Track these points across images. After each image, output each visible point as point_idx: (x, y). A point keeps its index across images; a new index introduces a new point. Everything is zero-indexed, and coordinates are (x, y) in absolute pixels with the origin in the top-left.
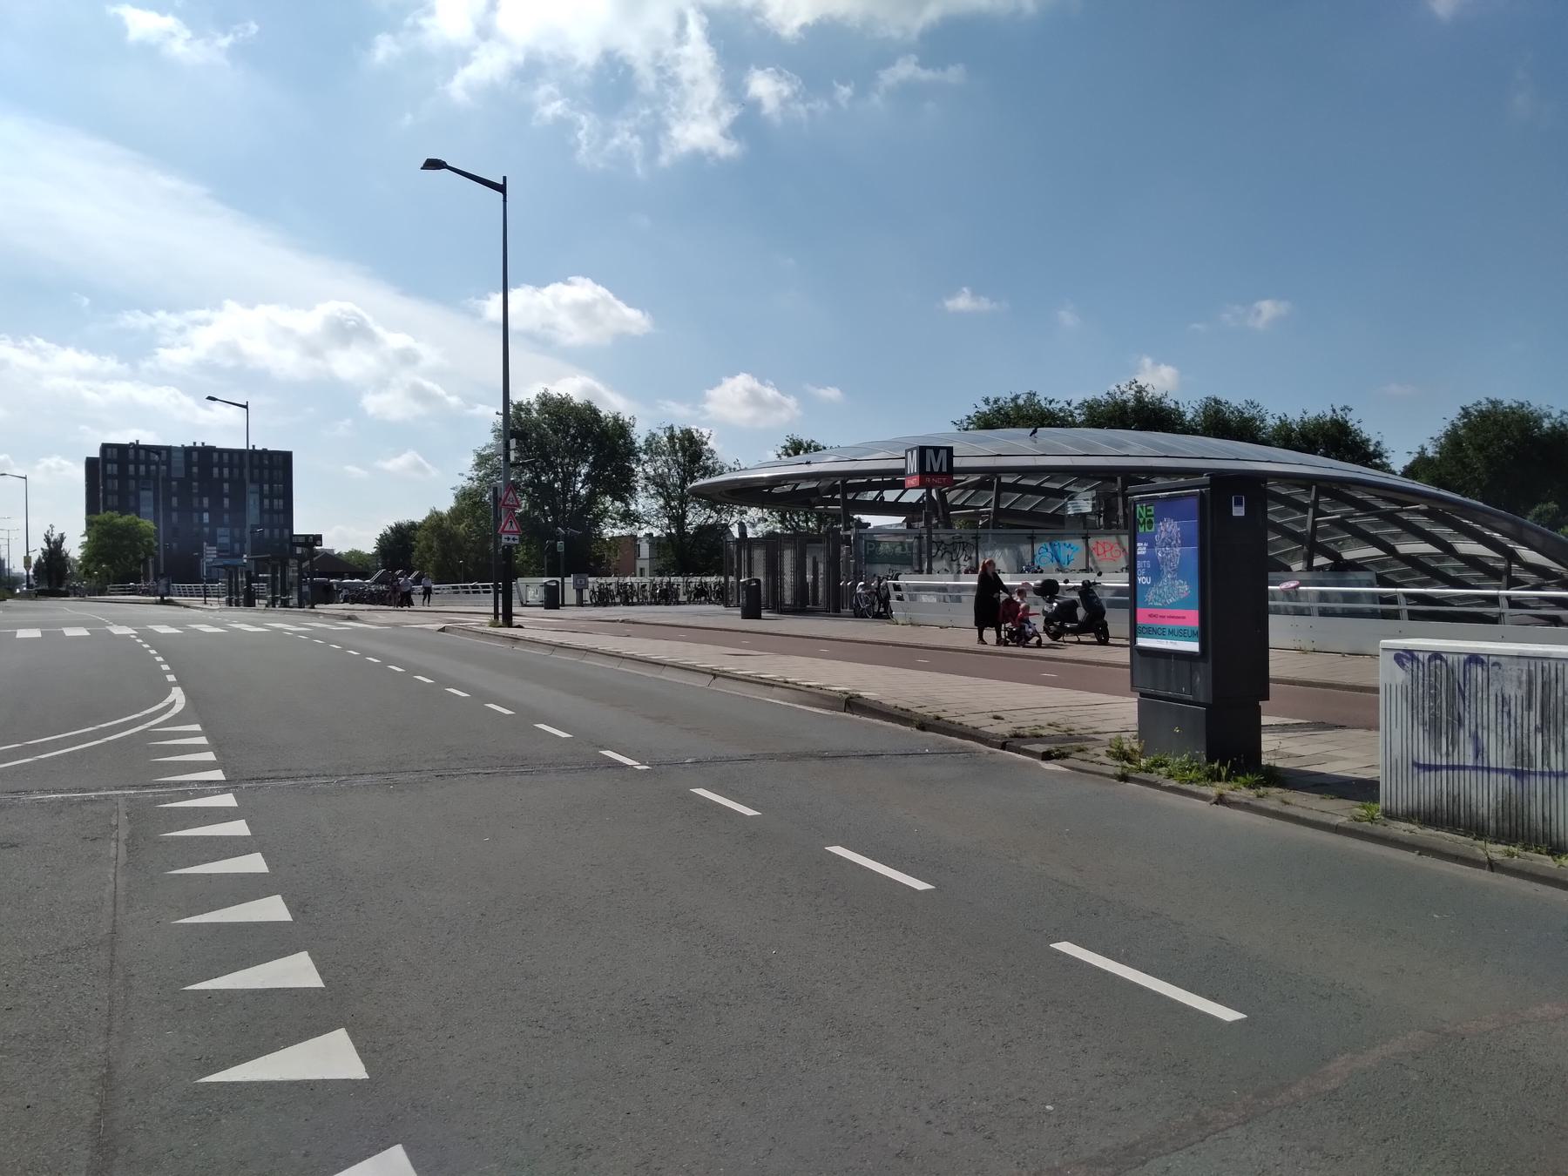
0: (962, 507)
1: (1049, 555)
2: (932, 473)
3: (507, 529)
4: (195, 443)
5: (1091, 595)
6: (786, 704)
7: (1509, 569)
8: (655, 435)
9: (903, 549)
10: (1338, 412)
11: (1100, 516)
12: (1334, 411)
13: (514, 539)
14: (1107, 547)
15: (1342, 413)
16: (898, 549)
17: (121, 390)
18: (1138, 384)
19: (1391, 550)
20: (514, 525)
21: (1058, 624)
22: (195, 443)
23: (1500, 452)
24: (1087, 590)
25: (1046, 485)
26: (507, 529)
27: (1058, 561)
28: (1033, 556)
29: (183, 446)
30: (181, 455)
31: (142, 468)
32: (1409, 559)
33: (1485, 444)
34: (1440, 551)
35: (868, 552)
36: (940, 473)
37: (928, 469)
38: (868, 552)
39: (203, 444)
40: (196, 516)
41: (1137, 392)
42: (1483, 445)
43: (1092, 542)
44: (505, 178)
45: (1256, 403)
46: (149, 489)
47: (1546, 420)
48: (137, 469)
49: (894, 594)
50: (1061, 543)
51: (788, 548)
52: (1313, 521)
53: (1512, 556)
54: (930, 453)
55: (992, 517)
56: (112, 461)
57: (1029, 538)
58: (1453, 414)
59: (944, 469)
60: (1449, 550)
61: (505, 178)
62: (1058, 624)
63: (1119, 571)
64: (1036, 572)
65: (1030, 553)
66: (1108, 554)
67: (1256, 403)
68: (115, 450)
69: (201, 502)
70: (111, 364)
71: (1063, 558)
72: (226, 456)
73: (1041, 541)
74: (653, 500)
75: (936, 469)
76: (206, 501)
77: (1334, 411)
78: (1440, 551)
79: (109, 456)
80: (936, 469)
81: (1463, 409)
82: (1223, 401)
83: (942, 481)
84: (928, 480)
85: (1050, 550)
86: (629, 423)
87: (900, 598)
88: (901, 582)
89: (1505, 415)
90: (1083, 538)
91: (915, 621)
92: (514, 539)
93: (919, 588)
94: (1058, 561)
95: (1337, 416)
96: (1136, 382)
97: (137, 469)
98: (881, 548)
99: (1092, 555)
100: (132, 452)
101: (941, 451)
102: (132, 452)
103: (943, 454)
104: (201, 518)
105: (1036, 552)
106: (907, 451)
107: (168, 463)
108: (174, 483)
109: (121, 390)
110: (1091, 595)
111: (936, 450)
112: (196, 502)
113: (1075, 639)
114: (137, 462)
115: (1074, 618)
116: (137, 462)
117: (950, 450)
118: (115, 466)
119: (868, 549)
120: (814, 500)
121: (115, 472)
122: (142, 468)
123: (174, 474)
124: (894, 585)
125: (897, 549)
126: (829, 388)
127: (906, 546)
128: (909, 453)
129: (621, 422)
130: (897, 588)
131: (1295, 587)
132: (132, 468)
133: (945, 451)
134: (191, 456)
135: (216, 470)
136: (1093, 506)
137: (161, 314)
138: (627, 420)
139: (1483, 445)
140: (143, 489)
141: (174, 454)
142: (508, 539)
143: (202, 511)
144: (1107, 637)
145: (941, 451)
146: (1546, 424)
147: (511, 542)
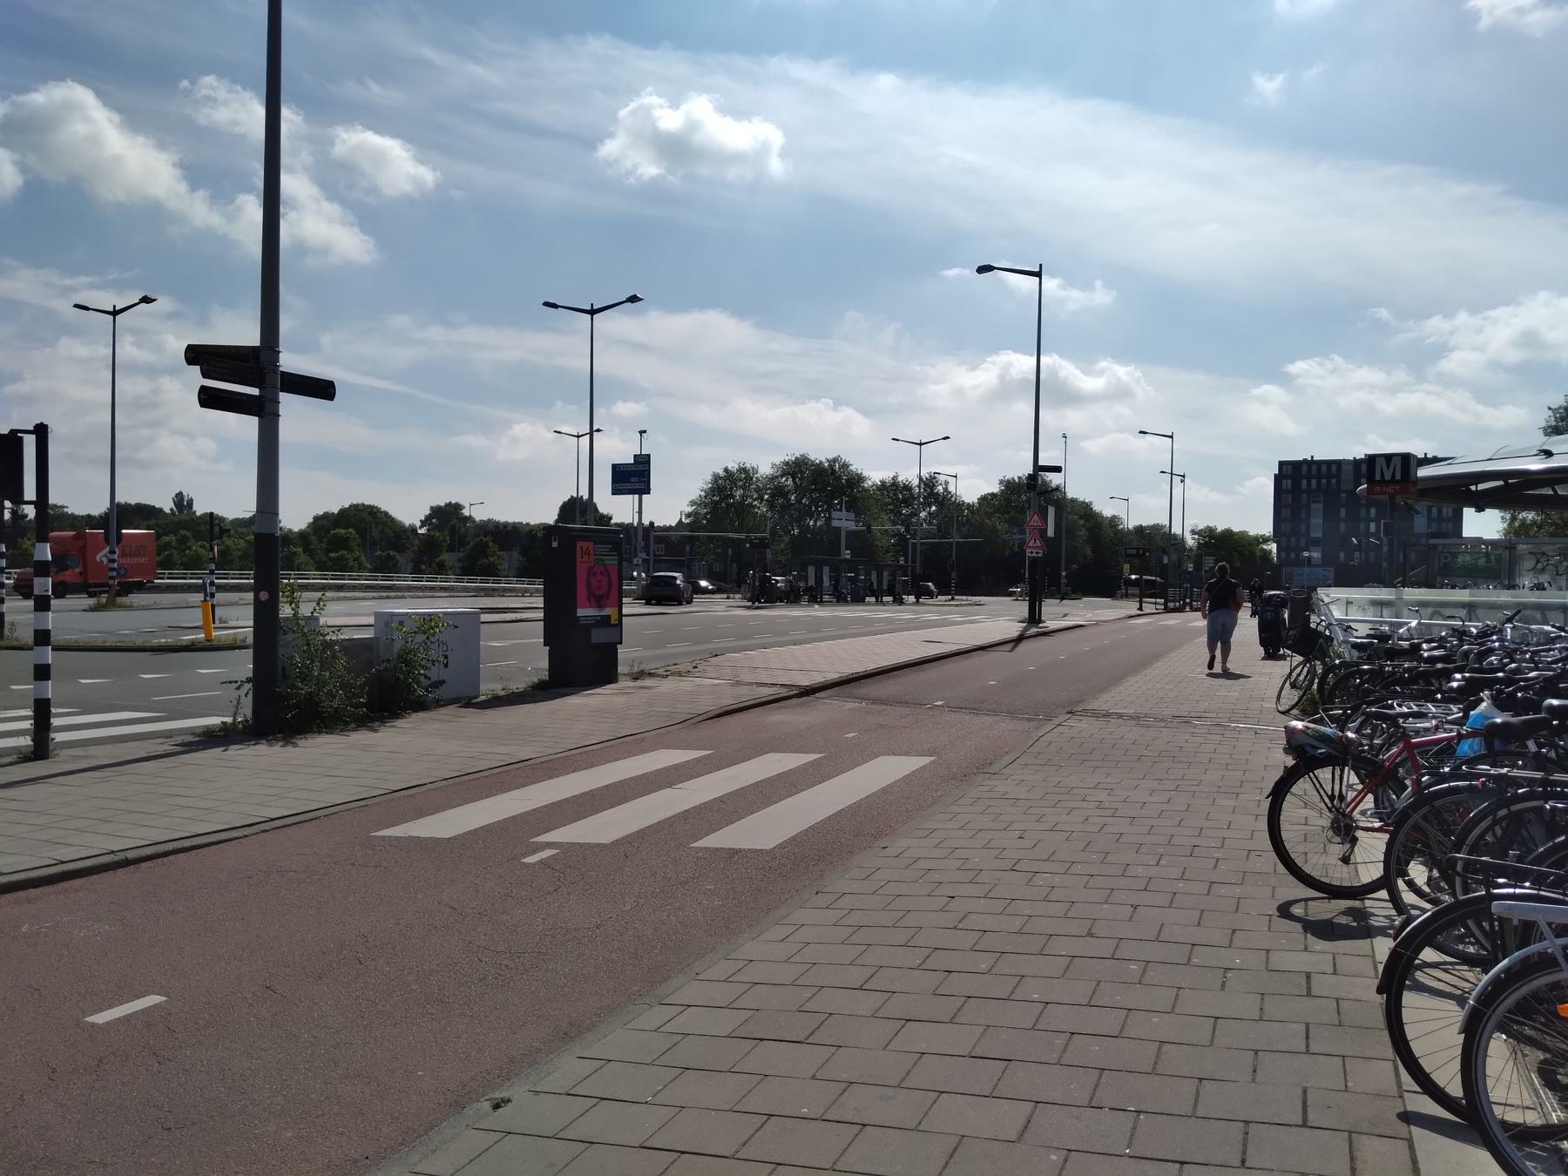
2: (1383, 481)
3: (1031, 544)
4: (1426, 454)
9: (1489, 561)
13: (1037, 553)
16: (1482, 562)
17: (1412, 400)
20: (1037, 541)
22: (1426, 454)
26: (1031, 544)
29: (1355, 458)
30: (1351, 467)
31: (1314, 482)
37: (1378, 477)
38: (1441, 565)
39: (1312, 457)
40: (1362, 526)
44: (1041, 265)
46: (1320, 502)
48: (1309, 483)
56: (1287, 478)
59: (1398, 477)
61: (1041, 265)
68: (1290, 467)
69: (1368, 512)
70: (1400, 376)
72: (1324, 468)
75: (1388, 477)
76: (1373, 511)
79: (1285, 473)
80: (1388, 477)
83: (1395, 489)
92: (1037, 553)
97: (1309, 483)
98: (1460, 559)
100: (1305, 467)
102: (1305, 467)
104: (1368, 528)
107: (1338, 476)
108: (1343, 495)
109: (1412, 400)
112: (1363, 511)
114: (1309, 477)
116: (1309, 477)
118: (1290, 481)
121: (1290, 487)
122: (1314, 482)
123: (1343, 487)
125: (1480, 561)
126: (1398, 395)
127: (1493, 557)
132: (1304, 482)
133: (1383, 459)
134: (1360, 467)
135: (1304, 482)
137: (1463, 317)
140: (1314, 502)
141: (1344, 468)
142: (1032, 553)
143: (1368, 520)
147: (1034, 555)
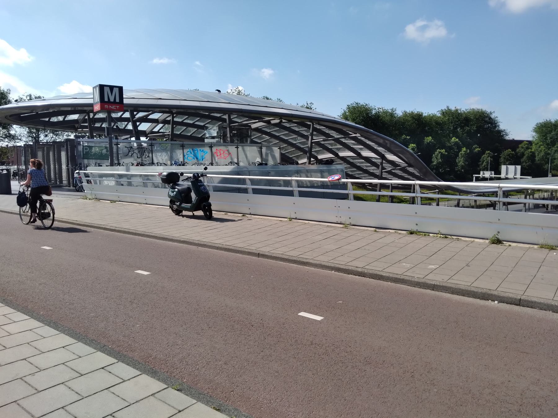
0: (158, 132)
1: (193, 156)
2: (109, 102)
5: (199, 184)
6: (152, 197)
7: (382, 163)
8: (22, 98)
10: (309, 104)
11: (221, 138)
12: (307, 104)
14: (222, 152)
15: (310, 105)
18: (239, 89)
19: (337, 155)
21: (178, 204)
23: (360, 121)
24: (196, 179)
25: (197, 123)
27: (197, 158)
28: (184, 156)
32: (344, 159)
33: (355, 118)
34: (356, 155)
35: (85, 153)
36: (115, 102)
37: (106, 99)
38: (85, 153)
41: (238, 92)
42: (354, 118)
43: (214, 149)
45: (281, 100)
47: (374, 111)
49: (84, 179)
50: (199, 149)
51: (63, 151)
52: (311, 142)
53: (383, 157)
54: (107, 90)
55: (170, 137)
57: (181, 146)
58: (345, 108)
59: (118, 100)
60: (359, 155)
62: (178, 204)
63: (228, 164)
64: (180, 165)
65: (182, 154)
66: (222, 156)
67: (281, 100)
71: (200, 157)
73: (188, 148)
74: (24, 130)
75: (112, 100)
77: (307, 104)
78: (356, 155)
80: (112, 100)
81: (348, 106)
82: (269, 98)
83: (116, 107)
84: (106, 106)
85: (192, 153)
86: (7, 92)
87: (89, 182)
88: (89, 171)
89: (361, 108)
90: (209, 147)
91: (98, 197)
93: (101, 176)
94: (197, 158)
95: (308, 106)
96: (238, 88)
99: (214, 156)
101: (115, 88)
103: (116, 91)
105: (185, 154)
106: (94, 88)
110: (199, 184)
111: (112, 88)
113: (190, 213)
115: (189, 200)
117: (121, 89)
119: (85, 151)
120: (76, 125)
124: (85, 173)
128: (95, 89)
129: (2, 91)
130: (87, 176)
131: (338, 179)
133: (118, 89)
136: (217, 132)
138: (6, 90)
139: (354, 118)
144: (210, 211)
145: (115, 88)
146: (374, 112)
